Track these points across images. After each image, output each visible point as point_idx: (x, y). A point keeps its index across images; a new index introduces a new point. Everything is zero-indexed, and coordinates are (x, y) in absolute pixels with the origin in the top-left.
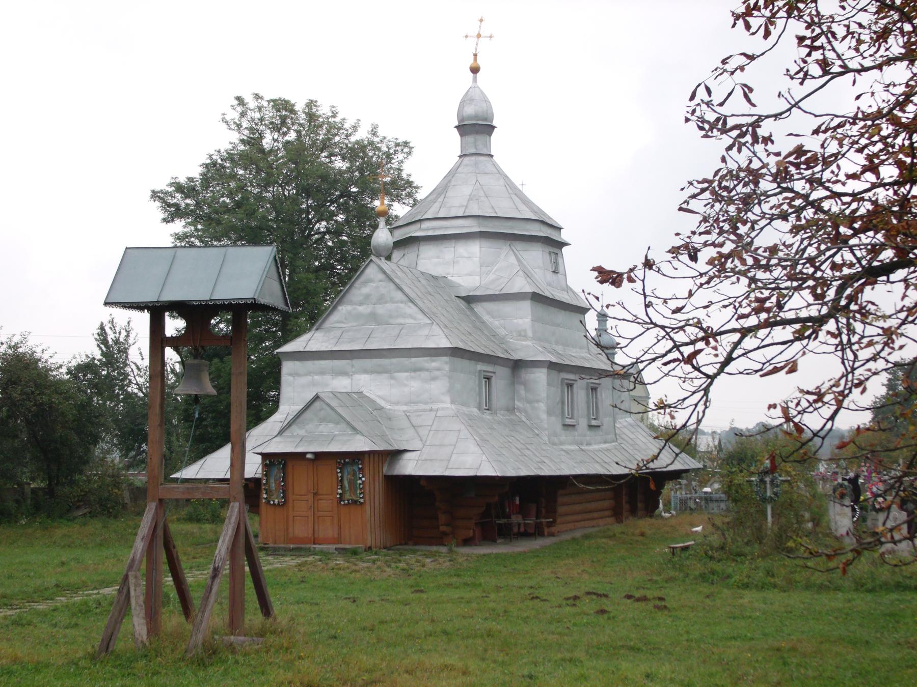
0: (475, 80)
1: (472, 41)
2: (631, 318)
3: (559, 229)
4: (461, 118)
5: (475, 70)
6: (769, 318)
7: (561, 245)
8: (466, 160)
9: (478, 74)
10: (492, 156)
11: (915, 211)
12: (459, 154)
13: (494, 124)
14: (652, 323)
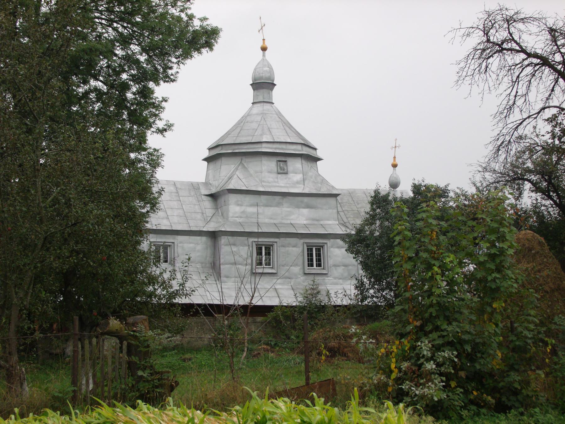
0: (264, 55)
1: (397, 145)
2: (511, 88)
3: (316, 149)
4: (254, 79)
5: (264, 49)
6: (458, 284)
7: (317, 159)
8: (255, 105)
9: (266, 52)
10: (273, 103)
11: (564, 147)
12: (252, 102)
13: (275, 82)
14: (523, 51)
